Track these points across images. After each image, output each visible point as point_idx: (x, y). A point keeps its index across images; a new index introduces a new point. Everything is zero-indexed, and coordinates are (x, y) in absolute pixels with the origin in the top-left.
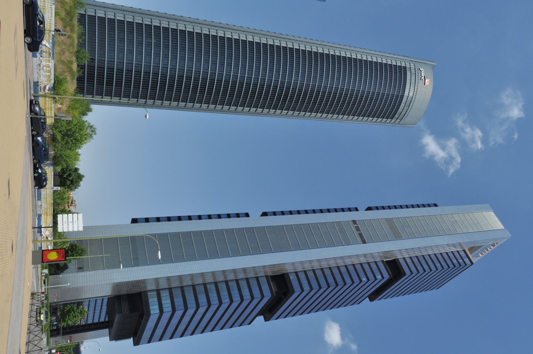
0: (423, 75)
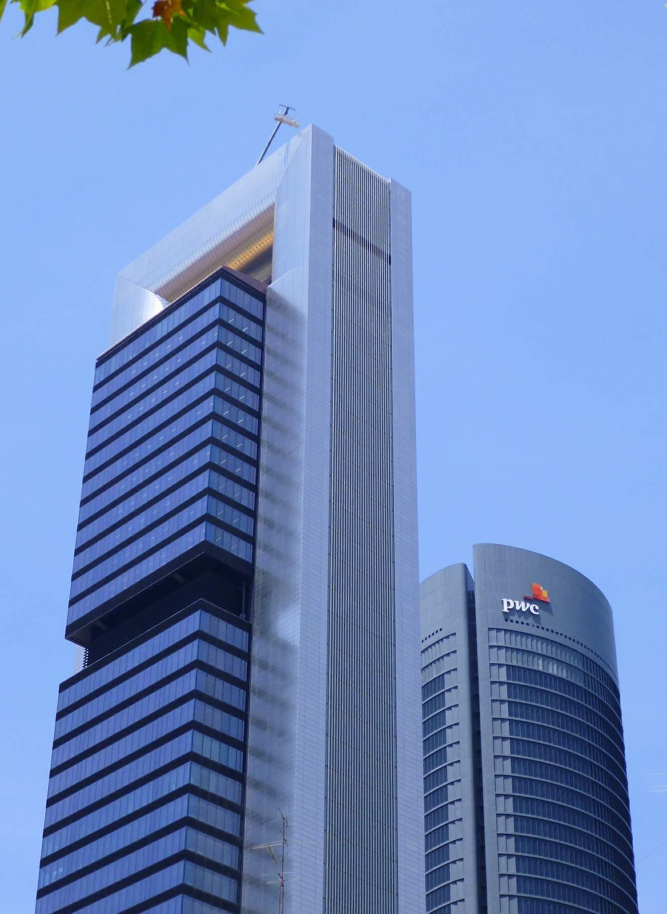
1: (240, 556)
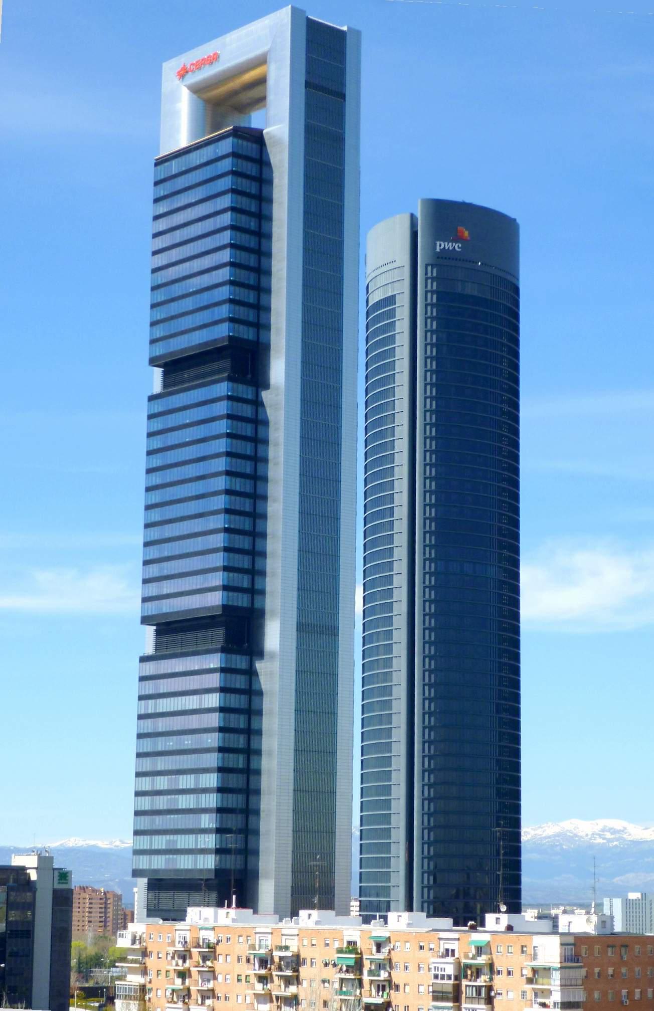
0: (450, 244)
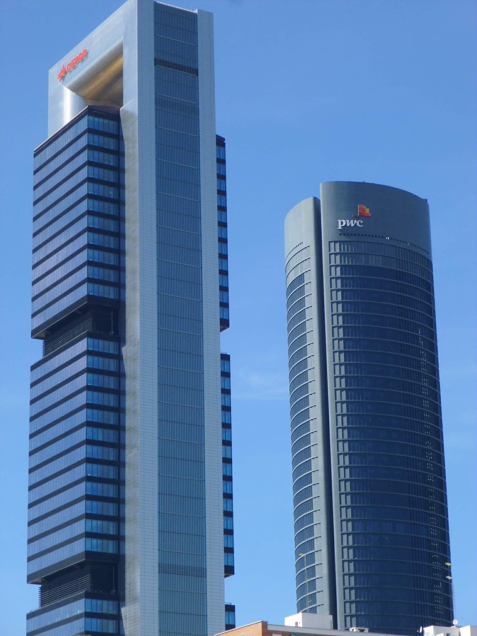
0: (352, 221)
1: (110, 297)
